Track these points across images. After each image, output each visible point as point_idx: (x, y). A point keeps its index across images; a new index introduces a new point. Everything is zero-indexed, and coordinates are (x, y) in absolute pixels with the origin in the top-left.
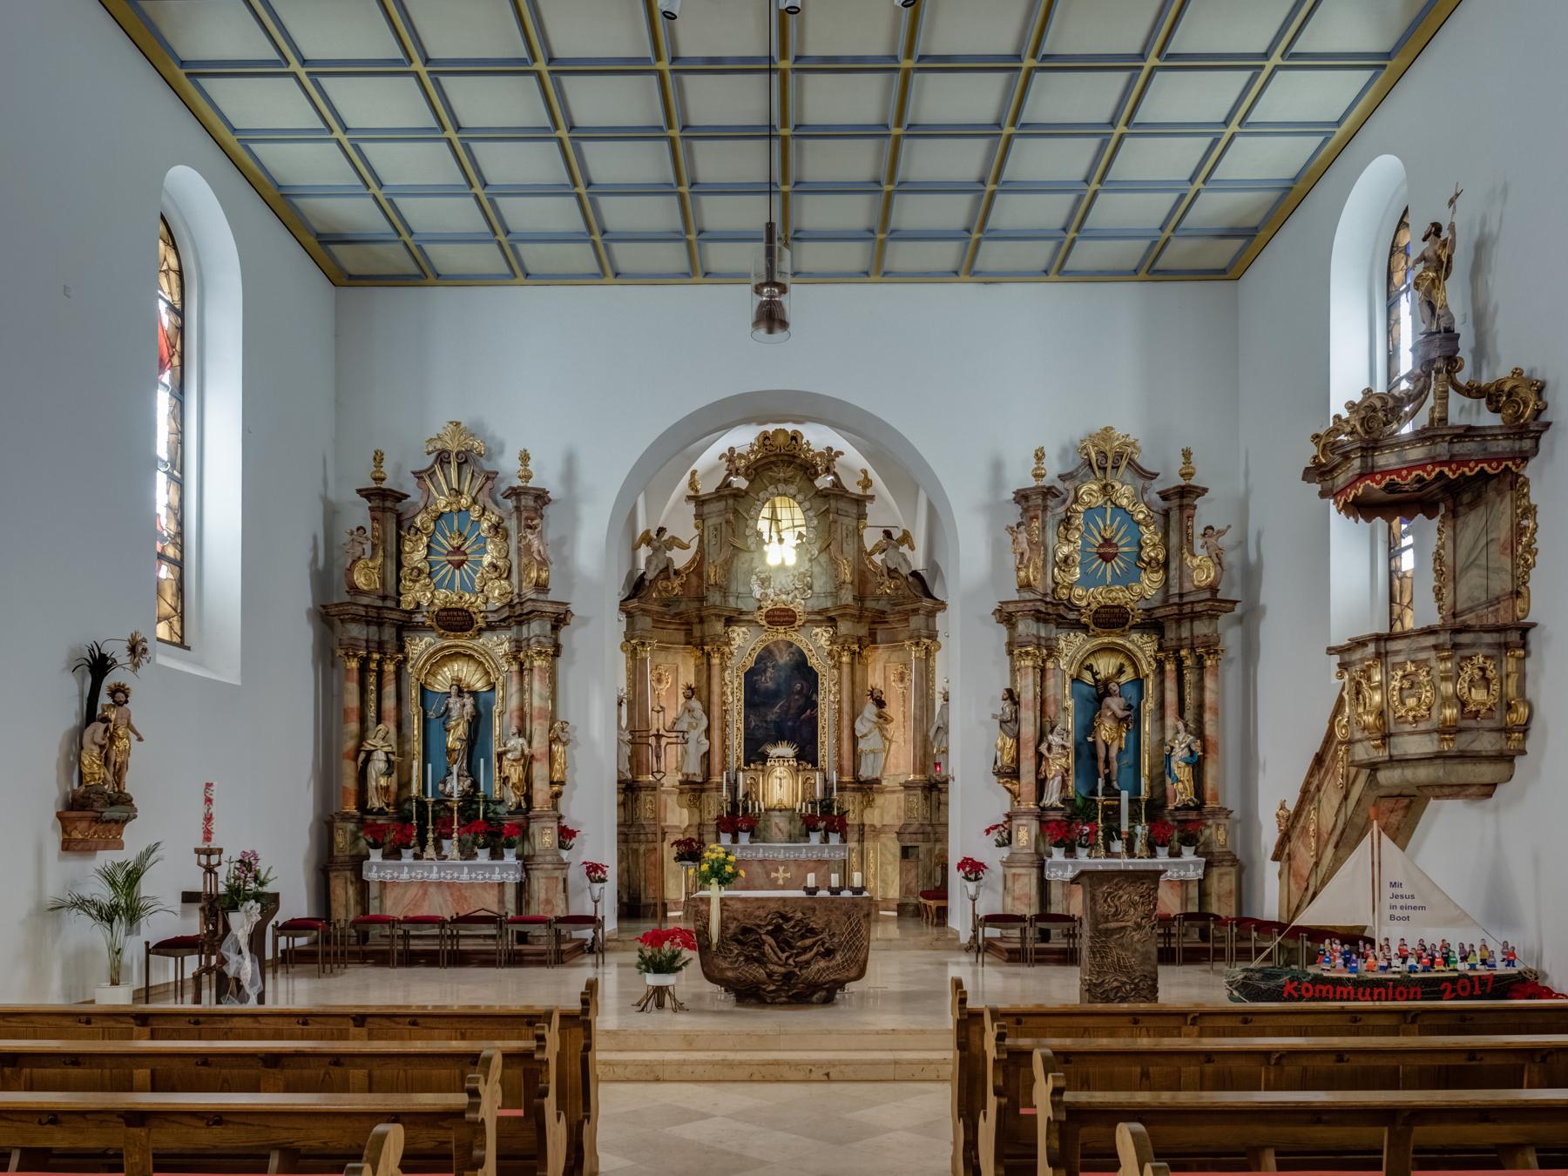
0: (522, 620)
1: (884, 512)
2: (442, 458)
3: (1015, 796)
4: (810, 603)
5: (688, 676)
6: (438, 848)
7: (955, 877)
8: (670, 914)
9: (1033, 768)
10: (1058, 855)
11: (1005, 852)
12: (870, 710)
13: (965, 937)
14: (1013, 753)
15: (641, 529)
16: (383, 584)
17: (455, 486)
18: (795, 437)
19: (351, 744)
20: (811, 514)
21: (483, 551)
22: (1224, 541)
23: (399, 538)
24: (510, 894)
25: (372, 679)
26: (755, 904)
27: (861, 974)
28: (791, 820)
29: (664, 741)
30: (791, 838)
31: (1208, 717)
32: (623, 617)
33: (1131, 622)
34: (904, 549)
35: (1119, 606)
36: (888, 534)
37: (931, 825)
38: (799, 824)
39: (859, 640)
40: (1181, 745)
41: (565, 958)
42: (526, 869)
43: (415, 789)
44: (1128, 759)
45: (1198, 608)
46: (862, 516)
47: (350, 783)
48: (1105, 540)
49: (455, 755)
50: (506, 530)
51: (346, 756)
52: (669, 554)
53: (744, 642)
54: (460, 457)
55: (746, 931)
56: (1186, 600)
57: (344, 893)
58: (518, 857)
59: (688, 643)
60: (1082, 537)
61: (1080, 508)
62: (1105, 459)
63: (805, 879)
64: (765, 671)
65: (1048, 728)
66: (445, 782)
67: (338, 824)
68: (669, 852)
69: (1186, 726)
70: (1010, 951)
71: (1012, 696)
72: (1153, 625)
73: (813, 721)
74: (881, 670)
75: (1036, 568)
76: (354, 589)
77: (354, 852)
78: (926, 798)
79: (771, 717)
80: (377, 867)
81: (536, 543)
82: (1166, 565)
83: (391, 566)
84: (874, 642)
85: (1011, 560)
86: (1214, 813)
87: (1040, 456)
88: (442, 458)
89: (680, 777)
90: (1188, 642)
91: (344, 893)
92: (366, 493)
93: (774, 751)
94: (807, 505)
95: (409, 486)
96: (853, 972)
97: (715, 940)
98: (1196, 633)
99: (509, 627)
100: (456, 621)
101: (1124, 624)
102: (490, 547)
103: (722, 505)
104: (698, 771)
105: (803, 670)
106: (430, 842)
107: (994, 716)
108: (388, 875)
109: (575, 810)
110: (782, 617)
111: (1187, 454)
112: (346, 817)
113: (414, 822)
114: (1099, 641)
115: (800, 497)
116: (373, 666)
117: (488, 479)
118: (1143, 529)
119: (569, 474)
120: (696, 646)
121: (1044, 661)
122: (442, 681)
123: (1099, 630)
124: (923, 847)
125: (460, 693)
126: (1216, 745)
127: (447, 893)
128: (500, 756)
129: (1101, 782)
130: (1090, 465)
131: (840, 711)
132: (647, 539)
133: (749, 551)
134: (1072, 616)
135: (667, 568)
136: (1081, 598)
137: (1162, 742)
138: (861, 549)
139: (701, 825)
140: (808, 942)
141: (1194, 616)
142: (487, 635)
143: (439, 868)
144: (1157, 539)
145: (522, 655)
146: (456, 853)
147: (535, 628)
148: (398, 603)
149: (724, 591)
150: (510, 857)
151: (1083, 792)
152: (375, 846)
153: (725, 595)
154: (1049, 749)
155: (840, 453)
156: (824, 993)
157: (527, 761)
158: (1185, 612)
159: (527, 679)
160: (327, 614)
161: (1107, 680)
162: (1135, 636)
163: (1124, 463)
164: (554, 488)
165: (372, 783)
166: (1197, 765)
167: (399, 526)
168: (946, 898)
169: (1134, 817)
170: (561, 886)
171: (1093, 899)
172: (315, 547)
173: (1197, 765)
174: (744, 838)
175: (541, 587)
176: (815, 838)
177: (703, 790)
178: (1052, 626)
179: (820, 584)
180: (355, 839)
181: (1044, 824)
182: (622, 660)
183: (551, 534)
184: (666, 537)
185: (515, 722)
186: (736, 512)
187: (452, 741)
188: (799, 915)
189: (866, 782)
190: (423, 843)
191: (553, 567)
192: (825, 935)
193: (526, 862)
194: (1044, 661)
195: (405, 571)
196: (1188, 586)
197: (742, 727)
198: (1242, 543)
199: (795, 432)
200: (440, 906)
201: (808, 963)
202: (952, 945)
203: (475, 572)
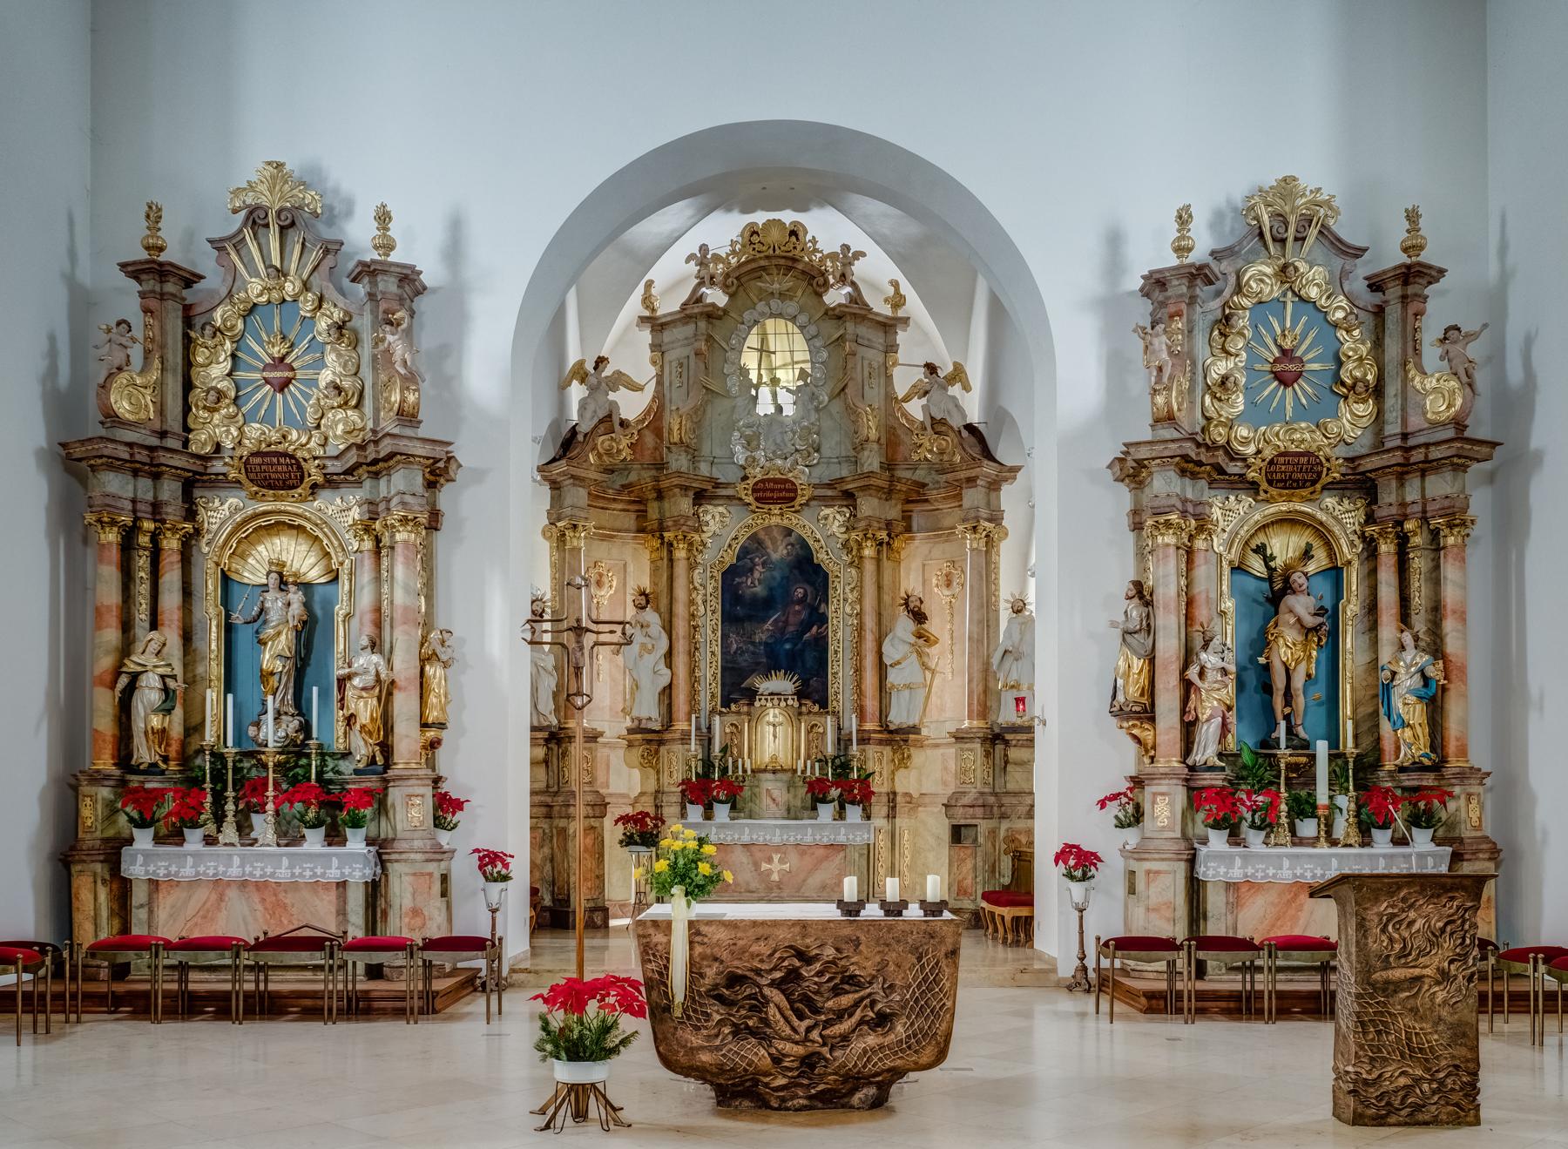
0: (378, 467)
1: (923, 340)
2: (256, 219)
3: (1148, 750)
4: (817, 472)
5: (640, 577)
6: (243, 828)
7: (1048, 877)
8: (613, 923)
9: (1177, 704)
10: (1218, 841)
11: (1131, 837)
12: (904, 626)
13: (1067, 969)
14: (1144, 680)
15: (573, 357)
16: (161, 412)
17: (276, 262)
18: (794, 233)
19: (106, 663)
20: (818, 343)
21: (320, 364)
22: (1474, 350)
23: (188, 343)
24: (356, 899)
25: (142, 562)
26: (751, 933)
27: (941, 1055)
28: (790, 786)
29: (589, 639)
30: (791, 813)
31: (1449, 625)
32: (546, 490)
33: (1325, 480)
34: (955, 390)
35: (1307, 454)
36: (931, 369)
37: (995, 794)
38: (802, 791)
39: (889, 525)
40: (1407, 668)
41: (438, 1003)
42: (382, 862)
43: (210, 736)
44: (1319, 691)
45: (1435, 453)
46: (891, 348)
47: (104, 722)
48: (1284, 352)
49: (274, 681)
50: (355, 332)
51: (99, 681)
52: (612, 396)
53: (722, 529)
54: (285, 217)
55: (734, 980)
56: (1411, 442)
57: (93, 899)
58: (370, 842)
59: (641, 530)
60: (1247, 347)
61: (1245, 302)
62: (1282, 226)
63: (840, 884)
64: (751, 570)
65: (1198, 641)
66: (258, 724)
67: (86, 789)
68: (613, 833)
69: (1416, 639)
70: (1151, 996)
71: (1141, 593)
72: (1360, 484)
73: (821, 644)
74: (919, 568)
75: (1180, 393)
76: (111, 418)
77: (110, 833)
78: (987, 754)
79: (761, 636)
80: (144, 857)
81: (399, 350)
82: (1378, 391)
83: (174, 386)
84: (908, 529)
85: (1139, 382)
86: (1463, 776)
87: (1184, 218)
88: (256, 219)
89: (628, 723)
90: (1417, 508)
91: (93, 899)
92: (134, 271)
93: (765, 686)
94: (813, 330)
95: (205, 262)
96: (927, 1054)
97: (679, 998)
98: (1429, 494)
99: (359, 483)
100: (276, 472)
101: (1314, 483)
102: (330, 358)
103: (689, 330)
104: (655, 714)
105: (807, 570)
106: (230, 818)
107: (1114, 624)
108: (160, 870)
109: (461, 768)
110: (776, 492)
111: (1412, 217)
112: (97, 778)
113: (208, 786)
114: (1272, 509)
115: (802, 319)
116: (144, 540)
117: (327, 251)
118: (1342, 334)
119: (454, 251)
120: (652, 532)
121: (1191, 538)
122: (253, 570)
123: (1274, 492)
124: (984, 826)
125: (283, 584)
126: (1463, 670)
127: (256, 898)
128: (342, 682)
129: (1281, 732)
130: (1261, 235)
131: (860, 628)
132: (580, 374)
133: (727, 395)
134: (1234, 468)
135: (610, 416)
136: (1246, 442)
137: (1374, 665)
138: (890, 397)
139: (658, 792)
140: (846, 1000)
141: (1427, 468)
142: (325, 494)
143: (243, 857)
144: (1363, 350)
145: (377, 525)
146: (271, 836)
147: (403, 482)
148: (186, 443)
149: (693, 453)
150: (356, 843)
151: (1250, 741)
152: (142, 824)
153: (694, 460)
154: (1202, 674)
155: (859, 255)
156: (872, 1091)
157: (385, 691)
158: (1413, 460)
159: (385, 563)
160: (69, 457)
161: (1288, 569)
162: (1330, 501)
163: (1313, 233)
164: (431, 272)
165: (138, 725)
166: (1434, 702)
167: (188, 322)
168: (1030, 903)
169: (1336, 781)
170: (437, 887)
171: (1362, 926)
172: (52, 354)
173: (1434, 702)
174: (722, 812)
175: (407, 416)
176: (826, 812)
177: (661, 743)
178: (1203, 483)
179: (834, 445)
180: (112, 811)
181: (1196, 797)
182: (544, 551)
183: (427, 339)
184: (608, 372)
185: (369, 629)
186: (710, 339)
187: (269, 659)
188: (829, 952)
189: (897, 731)
190: (219, 819)
191: (425, 386)
192: (876, 987)
193: (381, 847)
194: (1191, 538)
195: (197, 395)
196: (1415, 422)
197: (718, 651)
198: (1497, 357)
199: (795, 223)
200: (243, 921)
201: (845, 1038)
202: (1044, 978)
203: (307, 397)
